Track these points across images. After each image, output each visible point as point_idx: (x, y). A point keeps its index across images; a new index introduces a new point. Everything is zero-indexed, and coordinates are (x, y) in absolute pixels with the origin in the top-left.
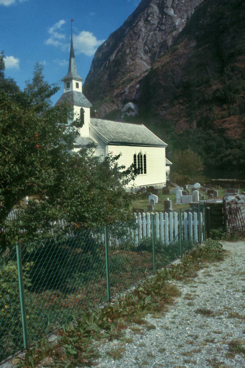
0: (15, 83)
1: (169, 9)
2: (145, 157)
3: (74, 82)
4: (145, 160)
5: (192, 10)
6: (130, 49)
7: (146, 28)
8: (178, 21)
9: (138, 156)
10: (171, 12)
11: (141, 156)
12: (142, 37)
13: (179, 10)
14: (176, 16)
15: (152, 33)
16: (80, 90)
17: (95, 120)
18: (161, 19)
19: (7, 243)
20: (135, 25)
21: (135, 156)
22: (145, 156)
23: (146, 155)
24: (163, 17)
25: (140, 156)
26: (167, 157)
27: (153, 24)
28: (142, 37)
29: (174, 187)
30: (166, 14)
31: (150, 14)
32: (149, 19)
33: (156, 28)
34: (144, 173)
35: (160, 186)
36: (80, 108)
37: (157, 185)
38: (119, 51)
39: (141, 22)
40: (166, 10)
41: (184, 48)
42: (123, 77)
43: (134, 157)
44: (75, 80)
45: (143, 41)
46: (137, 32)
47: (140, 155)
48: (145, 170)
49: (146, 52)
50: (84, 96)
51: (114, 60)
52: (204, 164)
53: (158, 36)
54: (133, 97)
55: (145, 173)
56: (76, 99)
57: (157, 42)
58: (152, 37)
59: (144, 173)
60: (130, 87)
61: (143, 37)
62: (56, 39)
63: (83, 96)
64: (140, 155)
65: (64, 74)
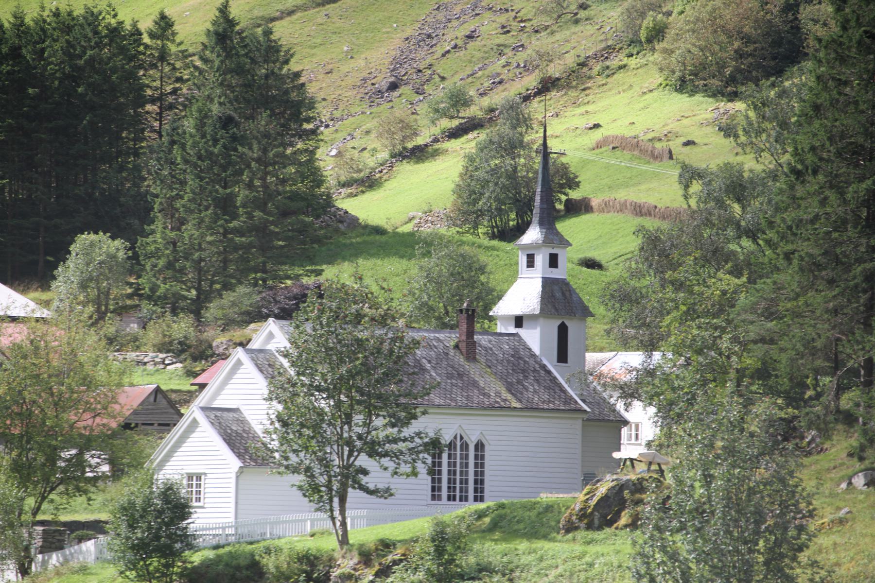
11: (465, 446)
22: (480, 446)
23: (485, 442)
34: (449, 499)
36: (559, 322)
47: (458, 444)
64: (458, 444)
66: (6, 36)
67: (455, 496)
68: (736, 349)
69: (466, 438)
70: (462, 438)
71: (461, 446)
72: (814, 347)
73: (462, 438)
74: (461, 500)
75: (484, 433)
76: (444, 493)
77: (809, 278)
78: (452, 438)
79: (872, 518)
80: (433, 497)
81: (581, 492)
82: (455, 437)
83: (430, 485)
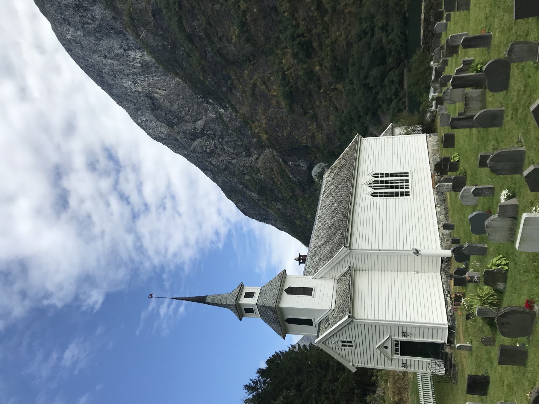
1: (197, 127)
4: (382, 175)
5: (198, 97)
6: (245, 174)
7: (219, 155)
8: (210, 115)
10: (200, 123)
11: (375, 182)
12: (231, 160)
13: (197, 114)
14: (204, 117)
15: (225, 147)
18: (208, 136)
19: (411, 95)
20: (216, 169)
21: (374, 195)
22: (375, 175)
24: (206, 134)
25: (374, 185)
27: (215, 147)
28: (231, 160)
30: (203, 130)
31: (203, 149)
32: (208, 151)
33: (220, 142)
34: (408, 176)
36: (285, 293)
38: (247, 187)
39: (212, 161)
40: (198, 130)
41: (242, 105)
43: (377, 196)
44: (239, 301)
45: (235, 158)
46: (224, 166)
47: (374, 185)
48: (401, 175)
49: (249, 155)
51: (259, 194)
52: (527, 367)
53: (230, 140)
55: (407, 174)
57: (236, 141)
58: (230, 147)
59: (408, 176)
60: (292, 174)
61: (231, 158)
64: (374, 185)
65: (230, 314)
66: (247, 21)
67: (406, 192)
68: (239, 95)
70: (370, 184)
71: (375, 184)
72: (178, 97)
73: (370, 184)
74: (407, 187)
75: (363, 183)
76: (404, 190)
77: (139, 187)
78: (371, 188)
79: (537, 68)
80: (408, 195)
81: (436, 68)
82: (370, 187)
83: (394, 197)
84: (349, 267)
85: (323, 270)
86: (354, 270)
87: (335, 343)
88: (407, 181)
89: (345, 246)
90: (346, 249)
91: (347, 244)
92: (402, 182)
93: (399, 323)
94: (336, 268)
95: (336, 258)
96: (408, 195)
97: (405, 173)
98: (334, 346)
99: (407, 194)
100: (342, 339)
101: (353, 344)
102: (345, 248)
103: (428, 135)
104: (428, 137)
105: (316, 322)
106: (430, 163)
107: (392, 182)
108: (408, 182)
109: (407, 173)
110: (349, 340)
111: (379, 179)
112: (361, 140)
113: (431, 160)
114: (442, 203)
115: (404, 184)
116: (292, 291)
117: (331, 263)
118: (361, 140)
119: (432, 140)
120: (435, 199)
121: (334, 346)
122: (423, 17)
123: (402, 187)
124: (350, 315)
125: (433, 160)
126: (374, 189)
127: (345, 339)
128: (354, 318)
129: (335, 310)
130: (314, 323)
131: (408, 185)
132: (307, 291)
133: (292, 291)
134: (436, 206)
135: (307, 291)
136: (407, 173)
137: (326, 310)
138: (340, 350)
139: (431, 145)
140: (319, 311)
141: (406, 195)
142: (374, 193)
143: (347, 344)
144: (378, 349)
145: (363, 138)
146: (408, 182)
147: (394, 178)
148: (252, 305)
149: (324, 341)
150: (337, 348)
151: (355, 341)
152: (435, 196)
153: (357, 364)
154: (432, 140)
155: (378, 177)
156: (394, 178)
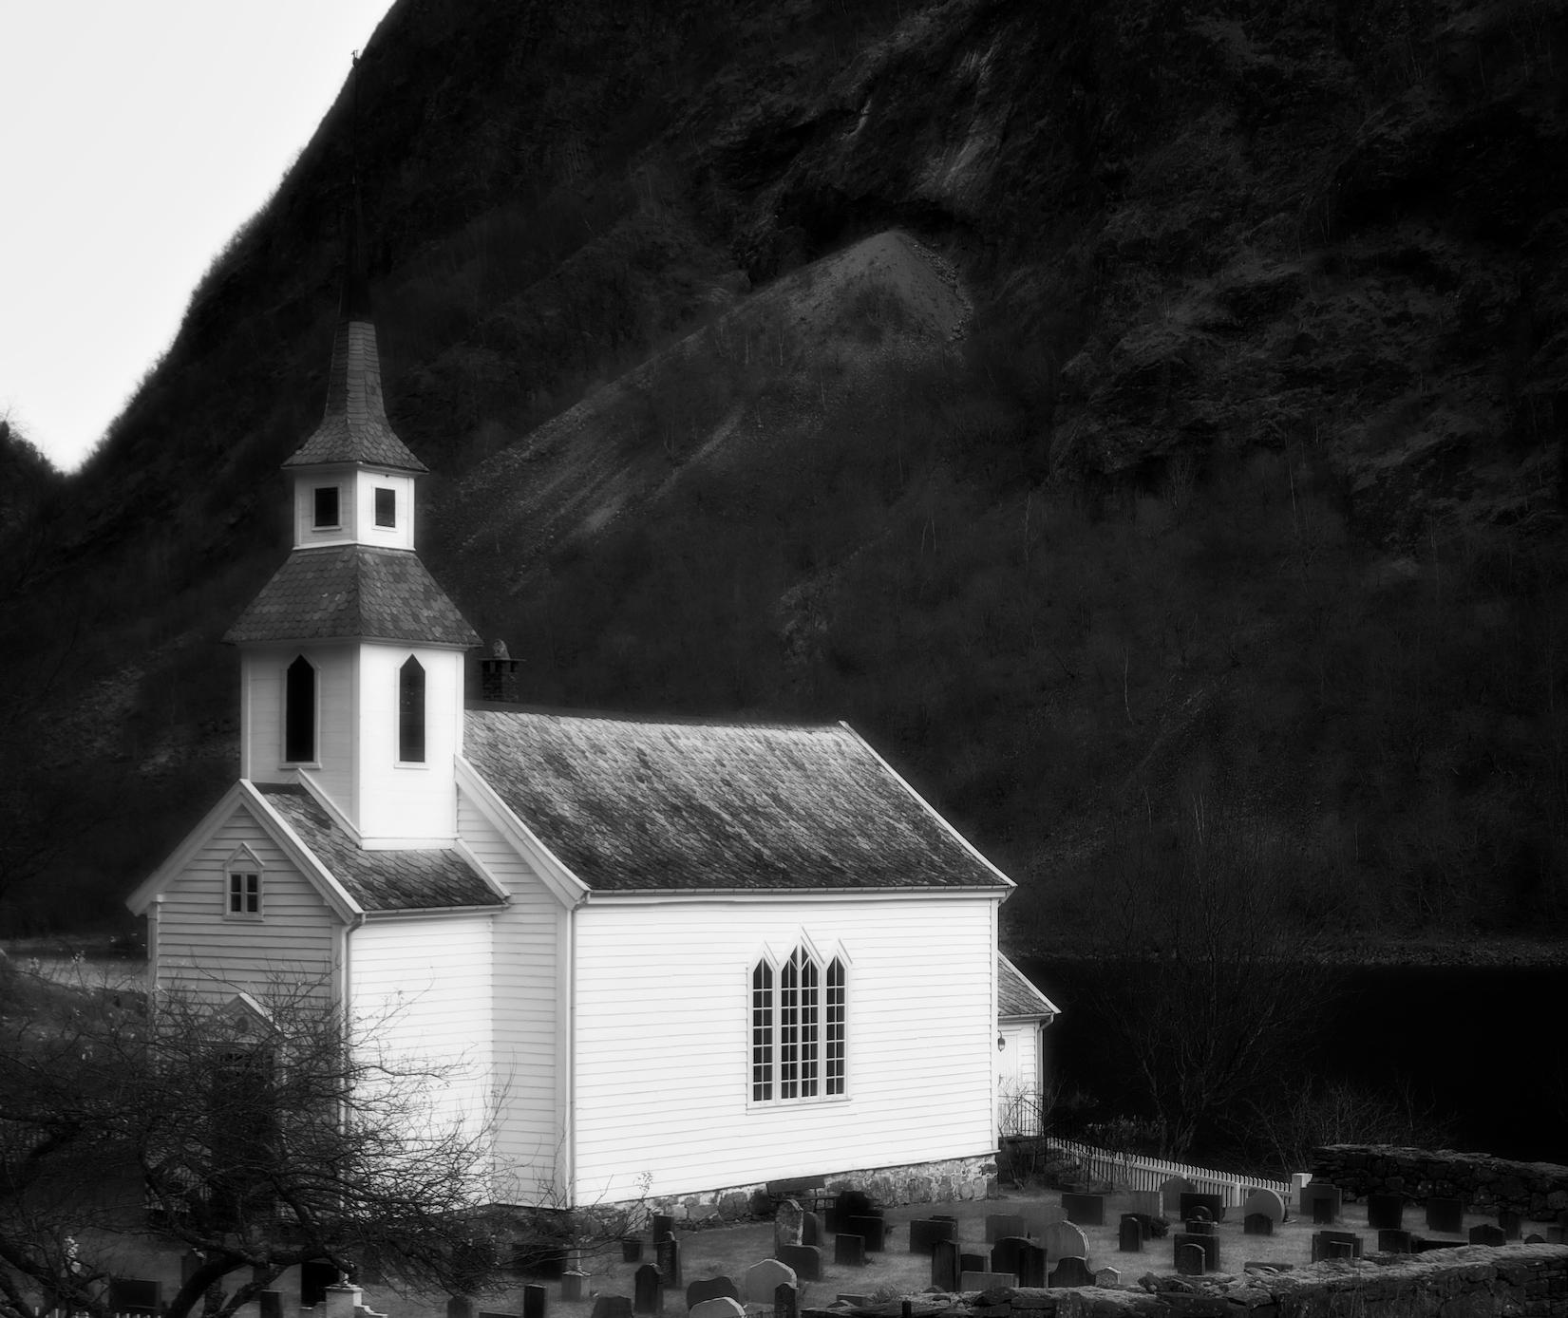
0: (35, 447)
2: (841, 982)
3: (366, 487)
4: (761, 1055)
9: (789, 974)
11: (810, 974)
16: (402, 536)
17: (508, 723)
21: (762, 976)
22: (836, 973)
25: (800, 973)
26: (1004, 944)
29: (1006, 1197)
35: (946, 1181)
37: (925, 1173)
42: (522, 793)
43: (757, 985)
44: (366, 470)
47: (800, 969)
48: (836, 1068)
50: (428, 580)
54: (406, 1250)
55: (835, 1086)
56: (379, 598)
59: (830, 1091)
62: (282, 1097)
63: (419, 577)
64: (800, 969)
67: (768, 1088)
69: (812, 957)
70: (805, 956)
71: (805, 972)
74: (788, 1091)
78: (789, 958)
80: (757, 1098)
82: (794, 956)
84: (507, 898)
85: (503, 815)
86: (492, 916)
87: (244, 850)
88: (810, 1089)
89: (586, 892)
90: (577, 895)
91: (593, 895)
92: (810, 1070)
93: (738, 1190)
94: (497, 848)
95: (545, 862)
96: (757, 1098)
97: (840, 1082)
98: (236, 845)
99: (761, 1092)
100: (262, 878)
101: (244, 914)
102: (582, 893)
103: (992, 1161)
104: (982, 1162)
105: (306, 776)
106: (875, 1170)
107: (810, 1034)
108: (805, 1094)
109: (840, 1090)
110: (263, 901)
111: (822, 988)
112: (991, 899)
113: (887, 1174)
114: (727, 1210)
115: (799, 1080)
116: (412, 682)
117: (522, 837)
118: (991, 899)
119: (971, 1177)
120: (741, 1190)
121: (236, 845)
122: (1382, 1148)
123: (788, 1072)
124: (364, 917)
125: (886, 1180)
126: (784, 973)
127: (263, 889)
128: (352, 930)
129: (359, 852)
130: (301, 766)
131: (794, 1095)
132: (412, 743)
133: (412, 682)
134: (717, 1191)
135: (412, 743)
136: (840, 1090)
137: (356, 820)
138: (218, 865)
139: (949, 1172)
140: (350, 792)
141: (757, 1089)
142: (768, 973)
143: (245, 894)
144: (235, 996)
145: (995, 905)
146: (805, 1094)
147: (822, 1042)
148: (352, 524)
149: (249, 813)
150: (225, 856)
151: (258, 923)
152: (752, 1189)
153: (159, 917)
154: (971, 1177)
155: (830, 982)
156: (822, 1042)
